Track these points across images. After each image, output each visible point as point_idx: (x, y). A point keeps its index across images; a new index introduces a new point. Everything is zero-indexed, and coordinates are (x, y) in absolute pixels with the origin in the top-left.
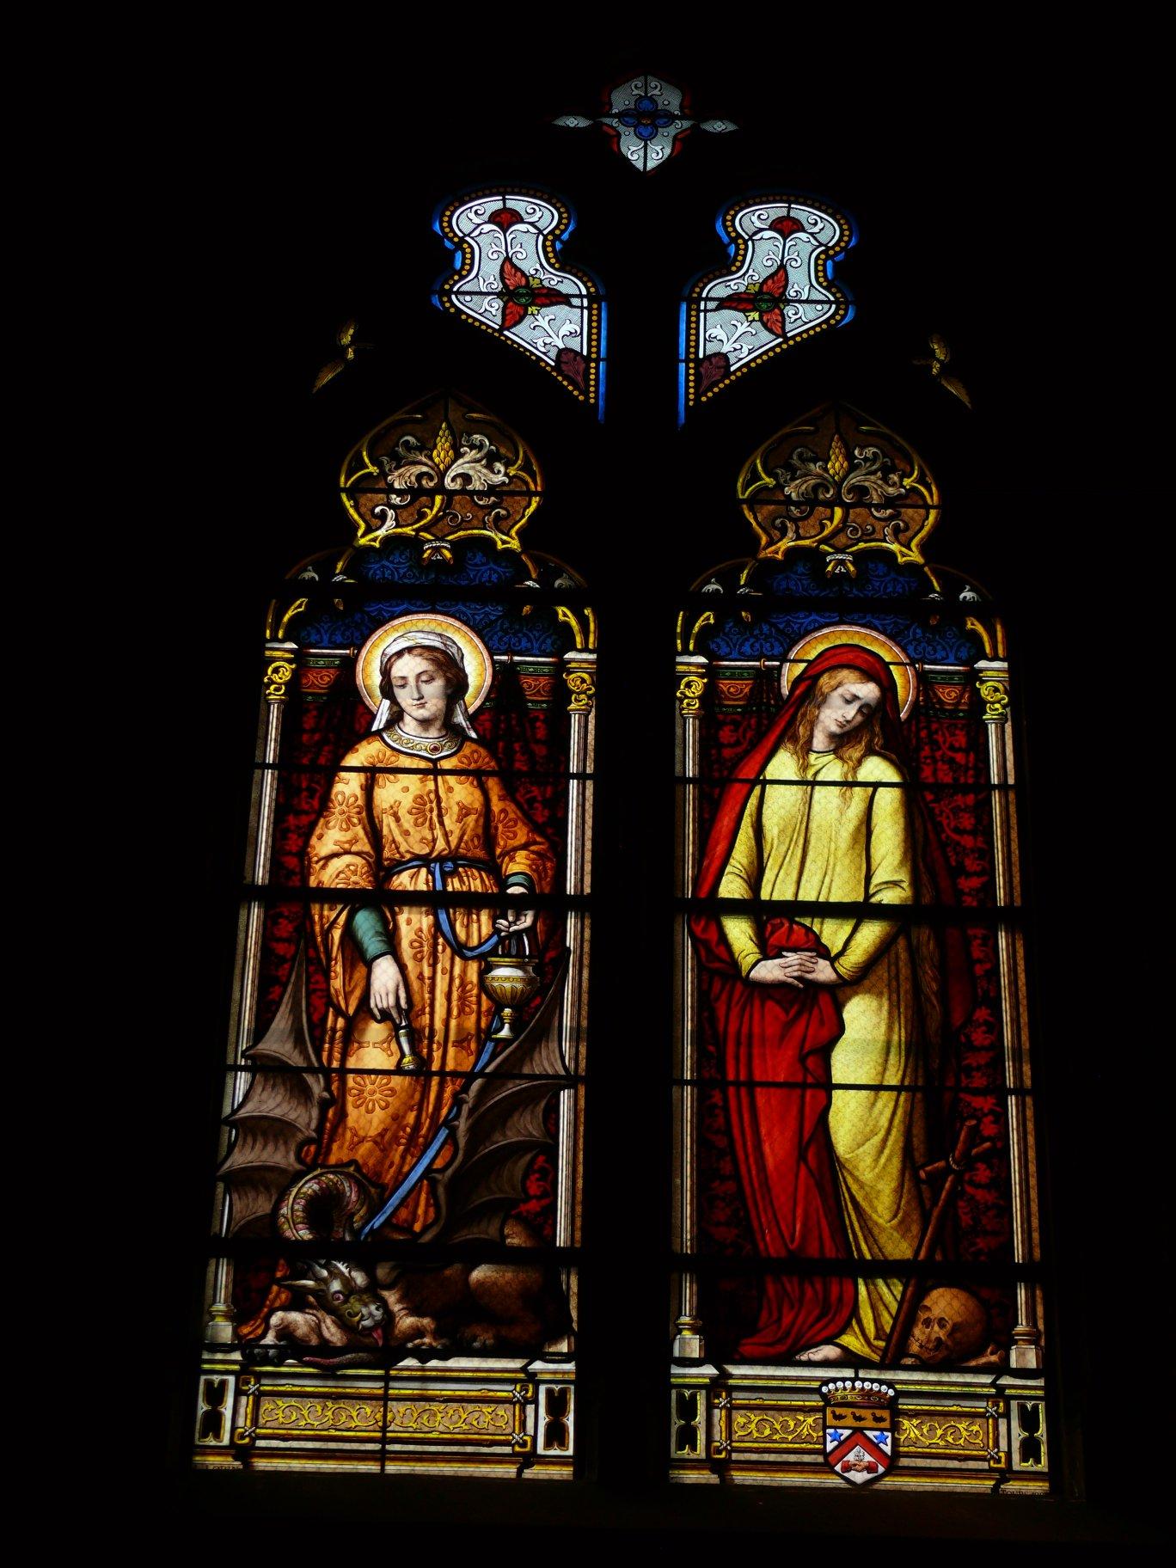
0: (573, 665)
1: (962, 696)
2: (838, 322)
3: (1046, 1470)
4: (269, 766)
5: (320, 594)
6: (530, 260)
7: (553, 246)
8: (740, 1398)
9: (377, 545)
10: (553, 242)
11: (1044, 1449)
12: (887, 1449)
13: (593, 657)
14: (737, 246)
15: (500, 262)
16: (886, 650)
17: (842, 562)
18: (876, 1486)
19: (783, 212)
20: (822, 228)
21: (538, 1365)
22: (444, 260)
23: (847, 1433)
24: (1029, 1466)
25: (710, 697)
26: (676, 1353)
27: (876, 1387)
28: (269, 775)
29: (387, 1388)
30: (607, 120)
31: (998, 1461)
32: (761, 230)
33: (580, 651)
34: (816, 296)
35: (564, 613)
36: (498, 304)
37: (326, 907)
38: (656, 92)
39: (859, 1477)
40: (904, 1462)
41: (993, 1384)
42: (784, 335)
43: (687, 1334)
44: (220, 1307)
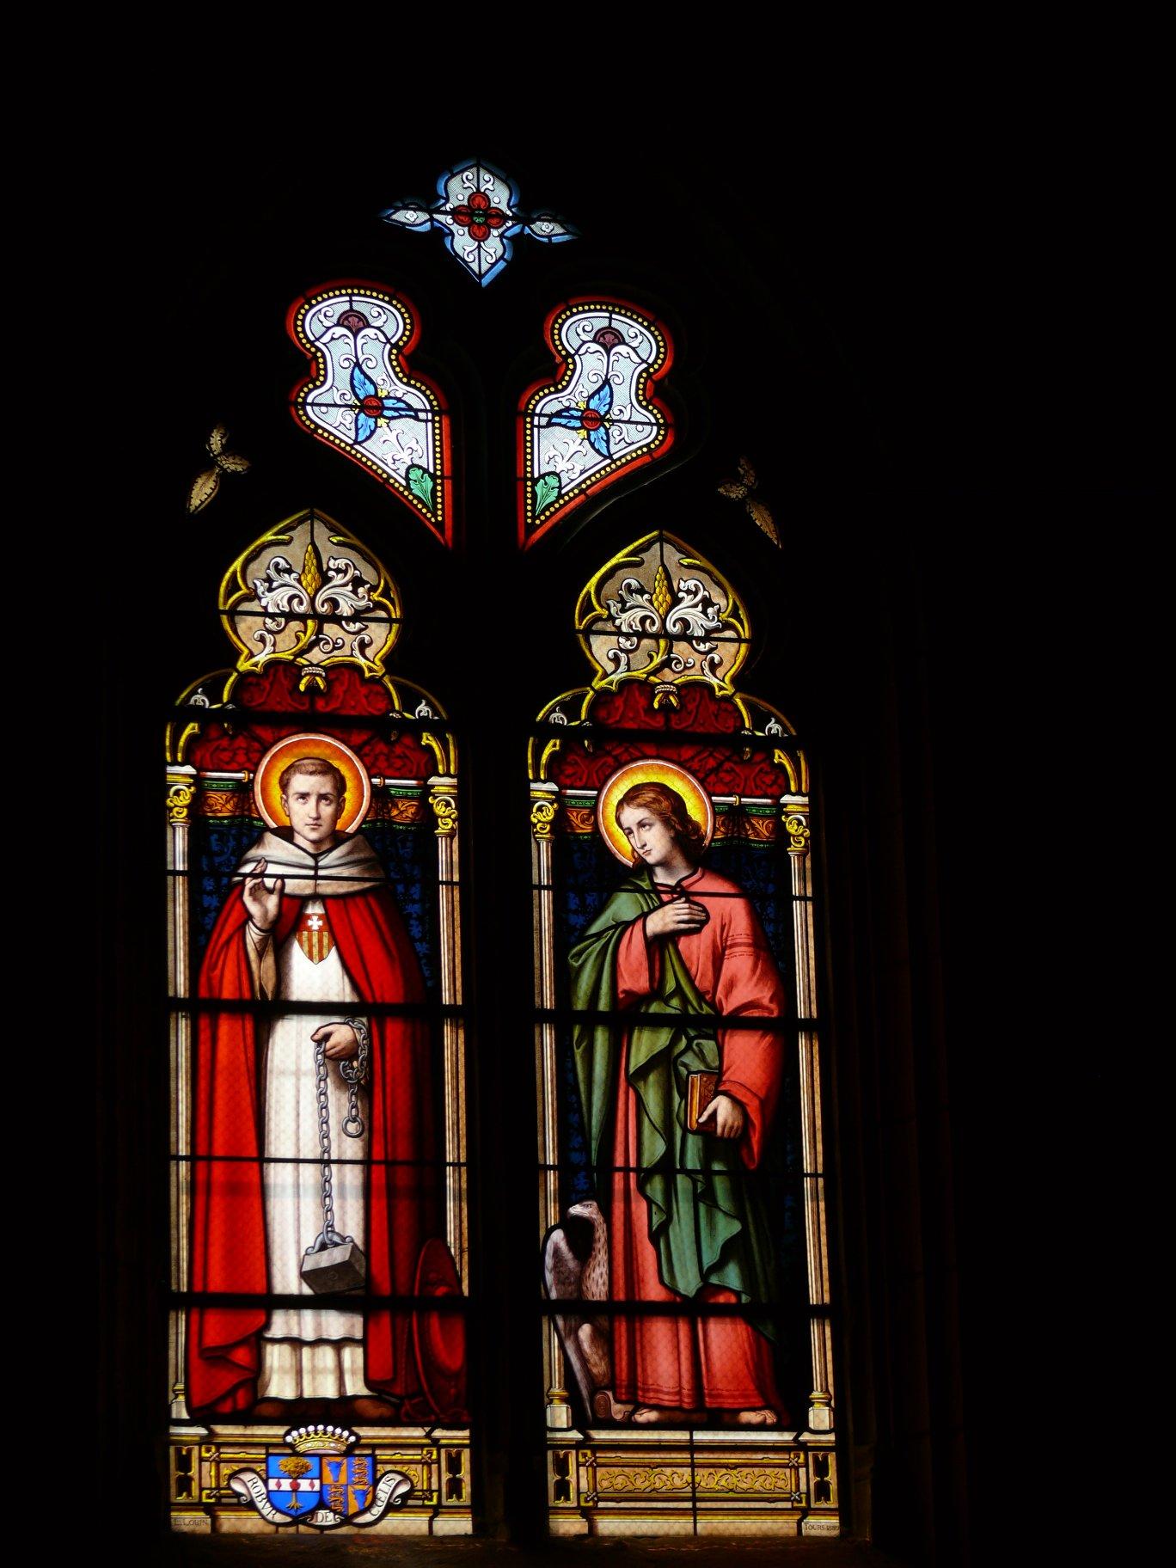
3: (468, 1503)
16: (681, 785)
24: (453, 1501)
26: (174, 1416)
34: (637, 417)
35: (427, 739)
37: (342, 1034)
38: (489, 185)
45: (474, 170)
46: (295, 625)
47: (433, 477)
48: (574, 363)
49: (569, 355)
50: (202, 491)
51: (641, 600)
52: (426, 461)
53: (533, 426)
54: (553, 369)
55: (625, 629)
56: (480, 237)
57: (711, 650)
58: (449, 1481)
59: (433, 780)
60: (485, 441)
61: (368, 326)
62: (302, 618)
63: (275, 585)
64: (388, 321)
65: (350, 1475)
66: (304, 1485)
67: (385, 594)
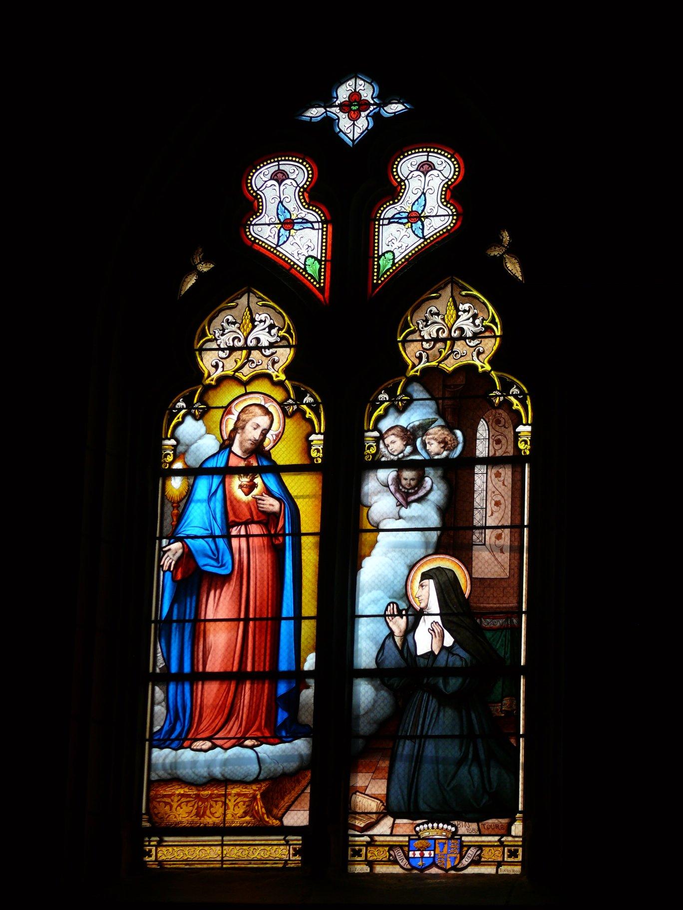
9: (418, 374)
13: (321, 437)
19: (425, 158)
20: (445, 168)
33: (525, 425)
45: (353, 80)
46: (439, 345)
47: (320, 261)
48: (405, 185)
49: (402, 181)
50: (513, 267)
52: (317, 253)
53: (379, 225)
54: (394, 192)
55: (426, 337)
56: (354, 119)
57: (273, 354)
59: (520, 428)
60: (351, 239)
61: (288, 178)
62: (444, 341)
63: (226, 331)
64: (298, 173)
65: (449, 848)
66: (426, 854)
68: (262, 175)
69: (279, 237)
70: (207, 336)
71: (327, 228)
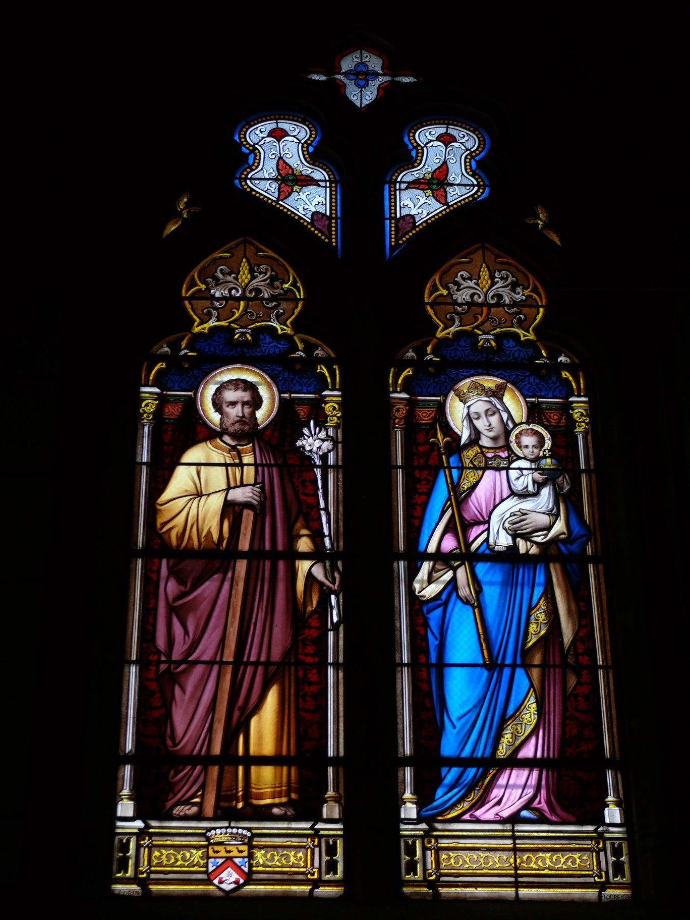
0: (327, 399)
1: (561, 419)
2: (479, 196)
3: (629, 881)
4: (400, 467)
5: (419, 364)
6: (297, 161)
7: (308, 150)
8: (444, 843)
10: (307, 148)
11: (626, 867)
12: (246, 870)
14: (417, 150)
15: (275, 162)
17: (488, 340)
18: (231, 895)
19: (274, 126)
20: (467, 139)
21: (319, 826)
22: (242, 159)
23: (221, 861)
25: (158, 414)
26: (403, 816)
27: (240, 831)
28: (400, 471)
29: (515, 844)
30: (338, 77)
31: (600, 877)
32: (431, 141)
34: (465, 182)
35: (565, 374)
36: (275, 185)
38: (367, 59)
39: (227, 887)
40: (255, 876)
41: (595, 831)
42: (446, 203)
43: (611, 806)
44: (126, 792)
45: (359, 52)
46: (476, 309)
51: (471, 284)
54: (408, 158)
58: (327, 862)
62: (238, 300)
67: (535, 290)
68: (258, 132)
69: (279, 192)
70: (438, 290)
71: (336, 187)
